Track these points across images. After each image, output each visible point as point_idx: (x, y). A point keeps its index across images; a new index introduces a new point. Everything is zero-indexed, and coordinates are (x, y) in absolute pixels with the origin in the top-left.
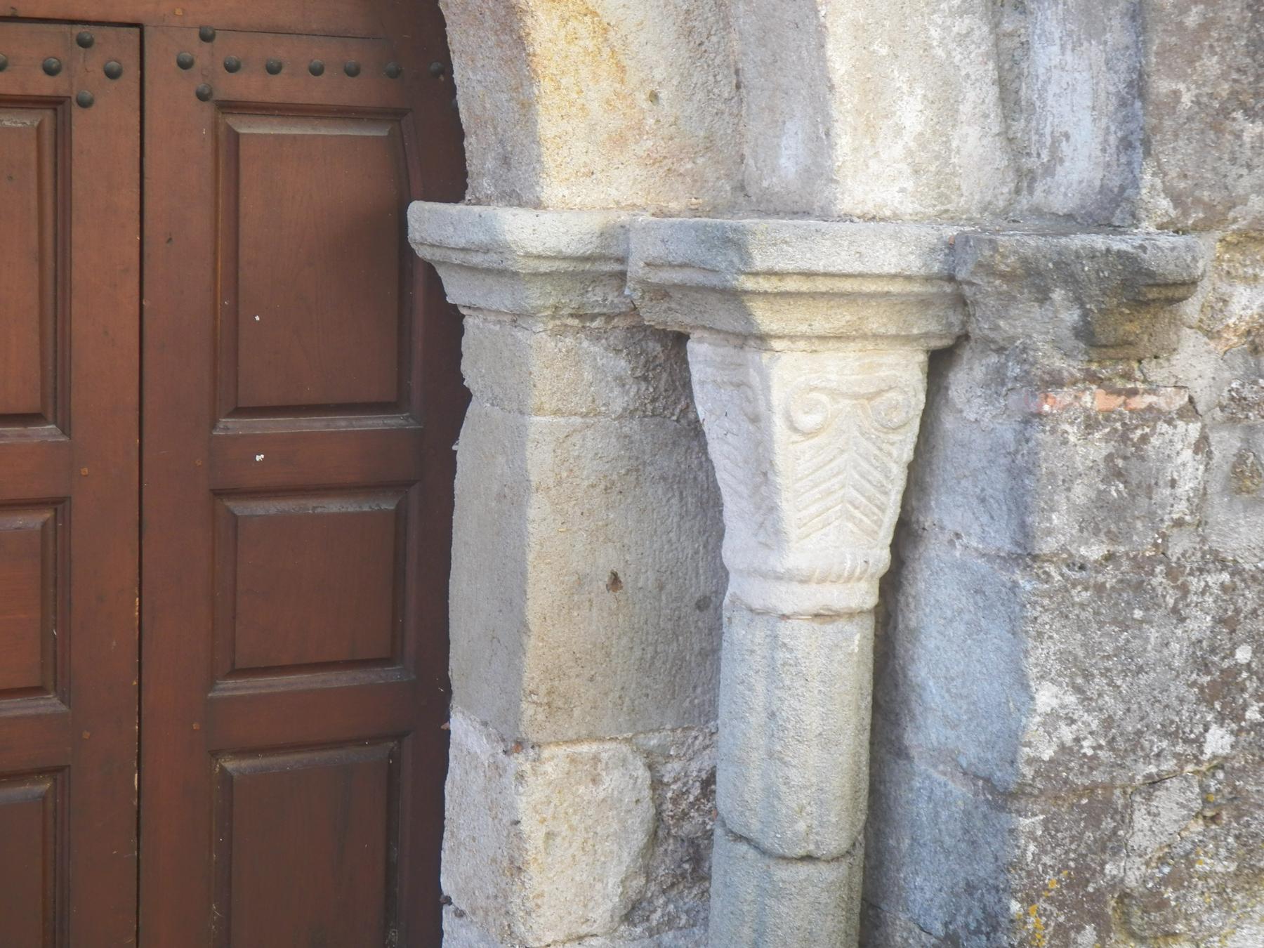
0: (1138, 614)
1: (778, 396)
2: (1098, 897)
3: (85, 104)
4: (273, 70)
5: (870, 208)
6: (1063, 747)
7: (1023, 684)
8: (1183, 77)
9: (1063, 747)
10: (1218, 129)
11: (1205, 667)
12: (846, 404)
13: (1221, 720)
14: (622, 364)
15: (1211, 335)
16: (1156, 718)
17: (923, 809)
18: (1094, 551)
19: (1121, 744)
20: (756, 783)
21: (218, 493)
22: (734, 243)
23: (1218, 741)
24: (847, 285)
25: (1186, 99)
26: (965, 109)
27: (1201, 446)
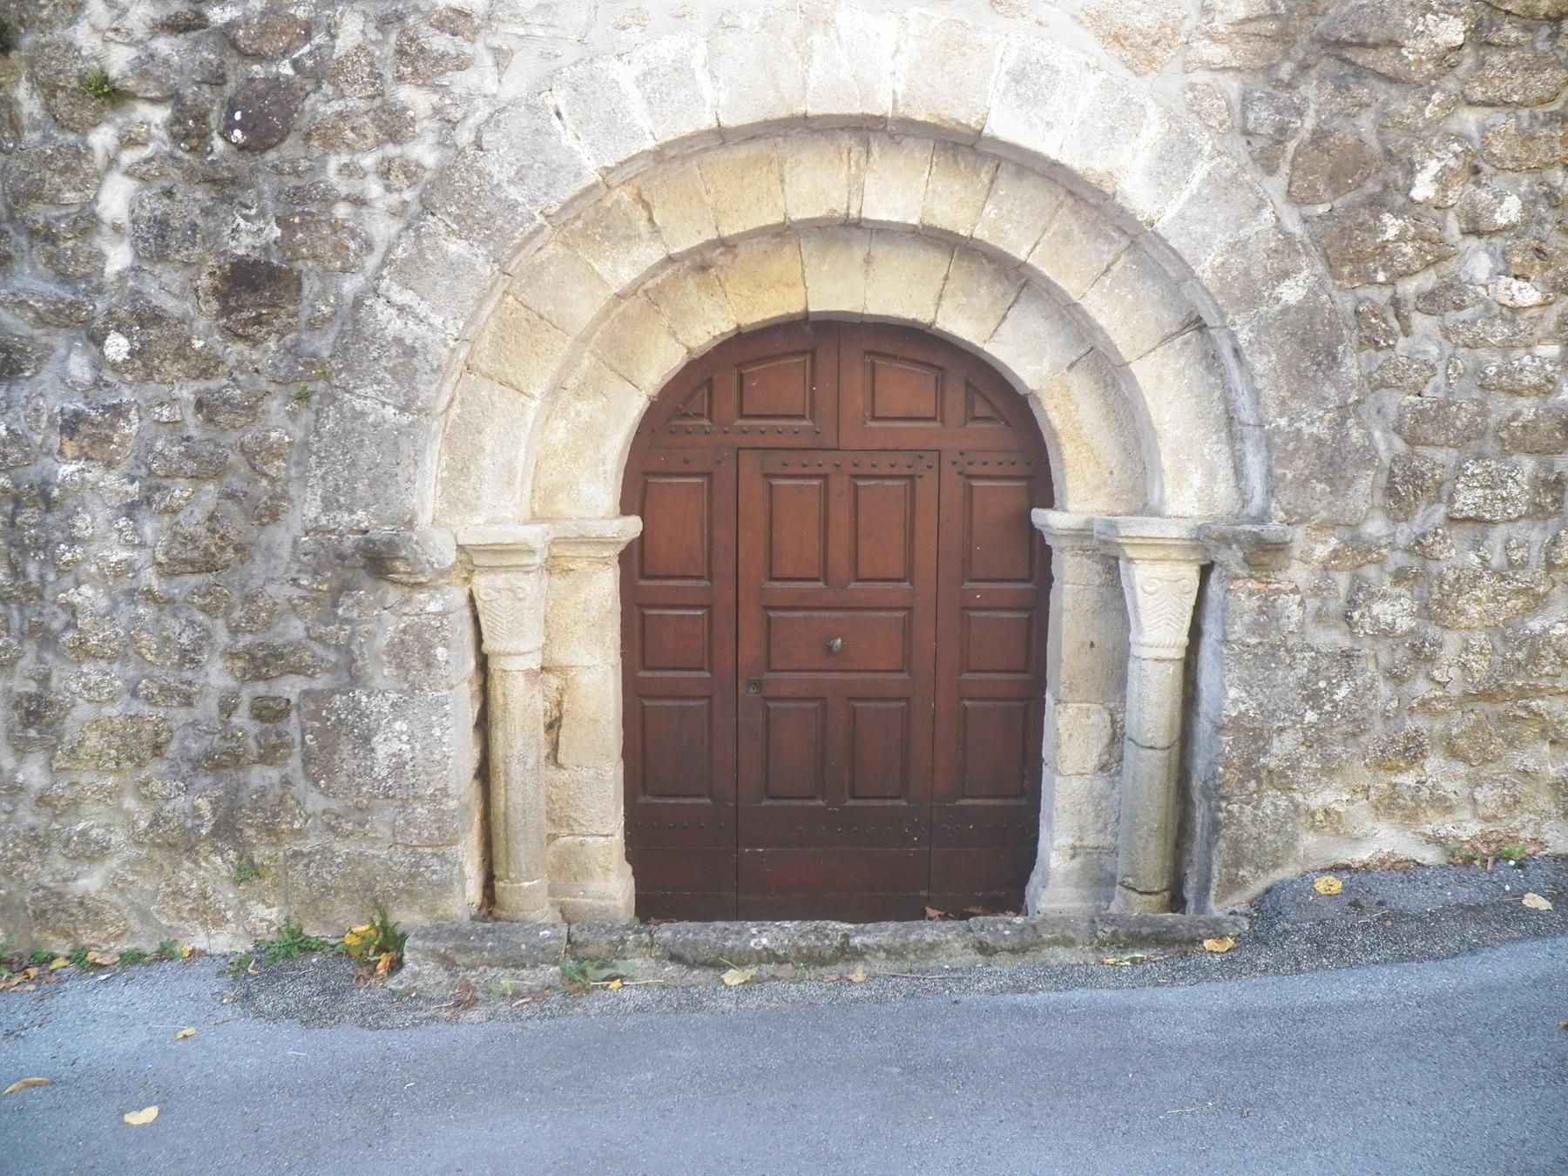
0: (1273, 665)
1: (1138, 580)
2: (1257, 770)
3: (920, 477)
4: (985, 464)
5: (1180, 513)
6: (1240, 712)
7: (1223, 687)
8: (1287, 468)
9: (1240, 712)
10: (1304, 486)
11: (1305, 688)
12: (1166, 583)
13: (1312, 708)
14: (1099, 567)
15: (1306, 562)
16: (1283, 706)
17: (1201, 735)
19: (1266, 713)
20: (1135, 719)
21: (964, 608)
23: (1311, 716)
24: (1159, 542)
25: (1289, 476)
26: (1220, 477)
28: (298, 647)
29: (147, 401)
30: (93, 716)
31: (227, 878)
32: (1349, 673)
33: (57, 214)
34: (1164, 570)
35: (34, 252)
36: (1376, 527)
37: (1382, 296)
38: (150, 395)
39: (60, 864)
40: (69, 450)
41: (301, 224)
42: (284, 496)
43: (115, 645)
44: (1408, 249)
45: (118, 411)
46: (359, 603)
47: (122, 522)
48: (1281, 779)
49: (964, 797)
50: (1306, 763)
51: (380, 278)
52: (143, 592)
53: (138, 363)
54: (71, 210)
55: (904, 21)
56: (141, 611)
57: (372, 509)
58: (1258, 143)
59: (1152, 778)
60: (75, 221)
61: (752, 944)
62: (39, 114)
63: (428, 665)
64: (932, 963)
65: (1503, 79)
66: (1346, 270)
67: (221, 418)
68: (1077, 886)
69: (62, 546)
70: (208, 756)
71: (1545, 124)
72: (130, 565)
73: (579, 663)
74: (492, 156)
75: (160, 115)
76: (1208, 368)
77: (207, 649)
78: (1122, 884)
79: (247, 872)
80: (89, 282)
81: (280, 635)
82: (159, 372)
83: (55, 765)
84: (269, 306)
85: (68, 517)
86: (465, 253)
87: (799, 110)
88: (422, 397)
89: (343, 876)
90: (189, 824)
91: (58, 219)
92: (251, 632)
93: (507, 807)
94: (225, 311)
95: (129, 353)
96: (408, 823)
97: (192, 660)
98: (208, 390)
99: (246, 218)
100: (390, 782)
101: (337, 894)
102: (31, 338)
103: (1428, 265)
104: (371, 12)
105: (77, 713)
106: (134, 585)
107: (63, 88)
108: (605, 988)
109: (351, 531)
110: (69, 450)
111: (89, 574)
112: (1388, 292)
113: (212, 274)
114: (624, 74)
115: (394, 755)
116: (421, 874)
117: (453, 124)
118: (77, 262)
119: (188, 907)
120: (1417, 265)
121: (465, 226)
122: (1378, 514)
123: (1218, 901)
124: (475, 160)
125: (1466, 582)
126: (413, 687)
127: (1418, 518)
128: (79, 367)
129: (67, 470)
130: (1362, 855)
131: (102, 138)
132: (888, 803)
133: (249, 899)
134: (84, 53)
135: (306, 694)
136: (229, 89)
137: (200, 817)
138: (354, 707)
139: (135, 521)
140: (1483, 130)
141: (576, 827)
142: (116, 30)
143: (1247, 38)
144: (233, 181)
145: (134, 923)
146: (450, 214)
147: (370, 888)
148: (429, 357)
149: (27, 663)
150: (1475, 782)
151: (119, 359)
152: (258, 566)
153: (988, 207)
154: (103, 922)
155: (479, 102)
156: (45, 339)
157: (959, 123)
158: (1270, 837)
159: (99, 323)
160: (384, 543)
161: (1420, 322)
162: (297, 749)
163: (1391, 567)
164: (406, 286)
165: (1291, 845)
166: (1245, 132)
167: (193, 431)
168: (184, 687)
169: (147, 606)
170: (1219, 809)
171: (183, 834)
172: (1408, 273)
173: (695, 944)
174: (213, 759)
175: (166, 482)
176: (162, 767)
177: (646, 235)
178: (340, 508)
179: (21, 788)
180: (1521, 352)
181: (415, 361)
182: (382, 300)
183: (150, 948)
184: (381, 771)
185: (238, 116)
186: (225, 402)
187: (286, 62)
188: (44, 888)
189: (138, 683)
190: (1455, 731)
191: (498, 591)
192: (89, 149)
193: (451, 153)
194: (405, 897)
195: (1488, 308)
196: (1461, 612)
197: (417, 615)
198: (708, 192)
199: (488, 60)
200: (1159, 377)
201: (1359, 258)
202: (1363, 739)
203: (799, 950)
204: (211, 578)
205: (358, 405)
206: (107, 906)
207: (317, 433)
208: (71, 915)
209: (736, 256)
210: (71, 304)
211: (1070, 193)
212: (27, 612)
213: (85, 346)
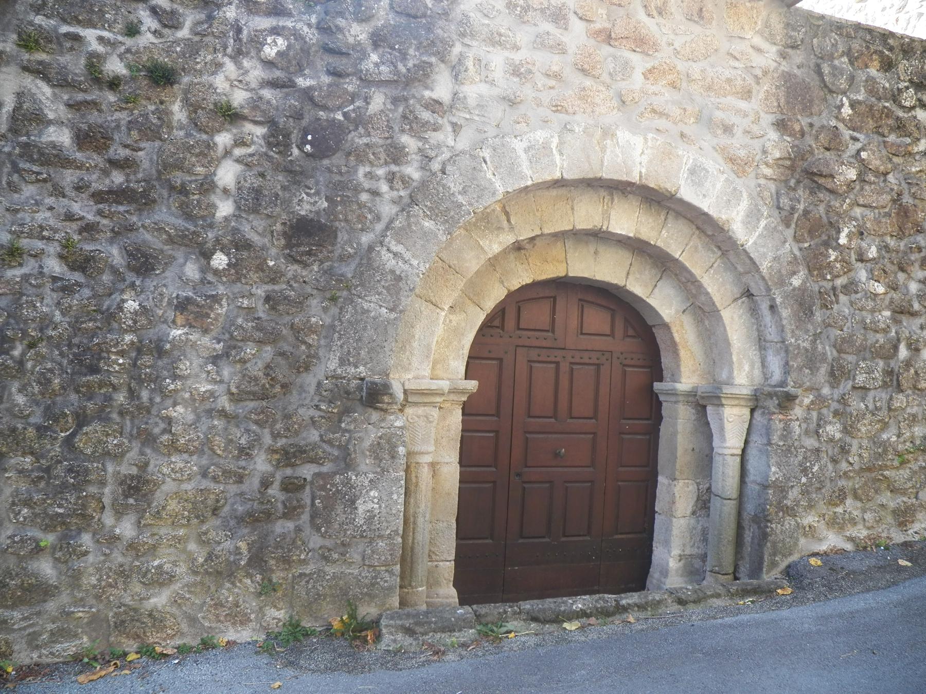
7: (769, 466)
14: (694, 411)
18: (781, 443)
22: (720, 389)
23: (804, 480)
27: (800, 426)
28: (315, 446)
29: (234, 294)
30: (175, 490)
31: (253, 593)
32: (818, 459)
33: (189, 179)
34: (736, 411)
35: (171, 199)
36: (826, 391)
37: (828, 285)
38: (236, 290)
39: (137, 588)
40: (179, 321)
41: (341, 201)
42: (316, 356)
43: (196, 444)
44: (838, 265)
45: (216, 299)
46: (355, 420)
47: (210, 367)
48: (790, 511)
49: (617, 534)
50: (802, 503)
51: (385, 236)
52: (218, 411)
53: (233, 271)
54: (199, 178)
55: (646, 139)
56: (216, 423)
57: (368, 366)
58: (784, 213)
59: (730, 514)
60: (202, 184)
61: (574, 607)
62: (184, 120)
63: (393, 457)
64: (660, 611)
65: (870, 196)
66: (815, 273)
67: (281, 308)
68: (682, 576)
69: (168, 380)
70: (250, 514)
71: (884, 217)
72: (212, 393)
73: (443, 461)
74: (451, 178)
75: (260, 131)
76: (751, 315)
77: (257, 447)
78: (711, 571)
79: (267, 589)
80: (204, 221)
81: (304, 439)
82: (246, 278)
83: (143, 522)
84: (317, 246)
85: (173, 362)
86: (432, 227)
87: (599, 175)
88: (403, 304)
89: (330, 587)
90: (232, 558)
91: (190, 182)
92: (286, 437)
93: (413, 543)
94: (289, 246)
95: (228, 265)
96: (373, 552)
97: (247, 454)
98: (274, 291)
99: (308, 194)
100: (365, 527)
101: (325, 599)
102: (162, 251)
103: (845, 273)
104: (389, 94)
105: (164, 488)
106: (213, 406)
107: (203, 109)
108: (507, 637)
109: (355, 378)
110: (179, 321)
111: (183, 399)
112: (831, 284)
113: (284, 224)
114: (519, 146)
115: (368, 511)
116: (378, 583)
117: (430, 159)
118: (200, 208)
119: (224, 614)
120: (841, 273)
121: (435, 213)
122: (827, 384)
123: (767, 574)
124: (442, 179)
125: (861, 416)
126: (383, 470)
127: (841, 387)
128: (192, 270)
129: (176, 333)
130: (823, 547)
131: (223, 139)
132: (581, 538)
133: (265, 606)
134: (218, 91)
135: (317, 475)
136: (305, 122)
137: (240, 554)
138: (347, 483)
139: (217, 367)
140: (863, 217)
141: (434, 557)
142: (240, 81)
143: (779, 166)
144: (301, 173)
145: (184, 627)
146: (426, 206)
147: (346, 594)
148: (409, 282)
149: (133, 455)
150: (864, 511)
151: (221, 268)
152: (294, 397)
153: (663, 232)
154: (165, 627)
155: (445, 149)
156: (170, 252)
157: (667, 190)
158: (788, 540)
159: (209, 245)
160: (382, 385)
161: (843, 298)
162: (308, 509)
163: (832, 409)
164: (399, 242)
165: (796, 544)
166: (779, 208)
167: (261, 315)
168: (241, 471)
169: (220, 420)
170: (767, 527)
171: (227, 565)
172: (838, 276)
173: (544, 610)
174: (254, 516)
175: (240, 344)
176: (218, 522)
177: (507, 229)
178: (349, 364)
179: (118, 538)
180: (877, 314)
181: (401, 284)
182: (385, 248)
183: (195, 642)
184: (360, 521)
185: (309, 137)
186: (286, 298)
187: (340, 112)
188: (124, 605)
189: (208, 468)
190: (857, 486)
191: (419, 417)
192: (215, 144)
193: (428, 174)
194: (367, 598)
195: (866, 294)
196: (859, 430)
197: (389, 428)
198: (538, 210)
199: (449, 129)
200: (732, 318)
201: (820, 269)
202: (823, 491)
203: (597, 609)
204: (264, 403)
205: (366, 306)
206: (168, 616)
207: (340, 320)
208: (144, 623)
209: (535, 245)
210: (194, 232)
211: (698, 228)
212: (136, 422)
213: (197, 258)
